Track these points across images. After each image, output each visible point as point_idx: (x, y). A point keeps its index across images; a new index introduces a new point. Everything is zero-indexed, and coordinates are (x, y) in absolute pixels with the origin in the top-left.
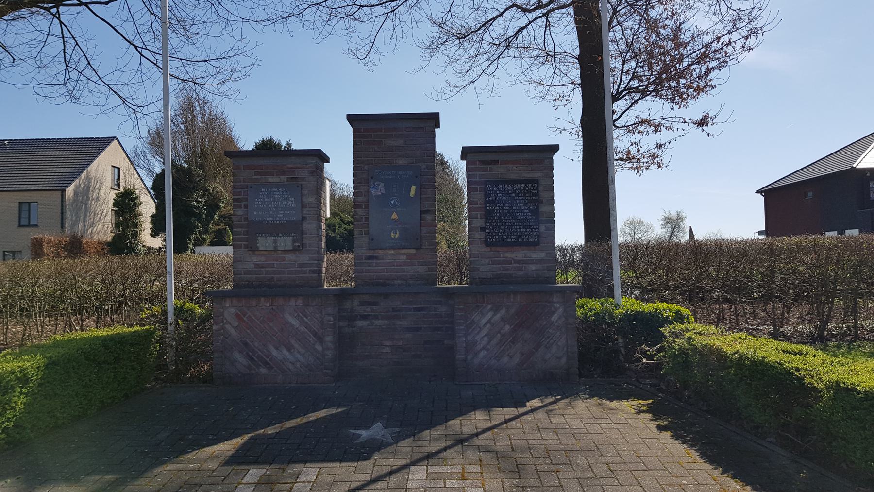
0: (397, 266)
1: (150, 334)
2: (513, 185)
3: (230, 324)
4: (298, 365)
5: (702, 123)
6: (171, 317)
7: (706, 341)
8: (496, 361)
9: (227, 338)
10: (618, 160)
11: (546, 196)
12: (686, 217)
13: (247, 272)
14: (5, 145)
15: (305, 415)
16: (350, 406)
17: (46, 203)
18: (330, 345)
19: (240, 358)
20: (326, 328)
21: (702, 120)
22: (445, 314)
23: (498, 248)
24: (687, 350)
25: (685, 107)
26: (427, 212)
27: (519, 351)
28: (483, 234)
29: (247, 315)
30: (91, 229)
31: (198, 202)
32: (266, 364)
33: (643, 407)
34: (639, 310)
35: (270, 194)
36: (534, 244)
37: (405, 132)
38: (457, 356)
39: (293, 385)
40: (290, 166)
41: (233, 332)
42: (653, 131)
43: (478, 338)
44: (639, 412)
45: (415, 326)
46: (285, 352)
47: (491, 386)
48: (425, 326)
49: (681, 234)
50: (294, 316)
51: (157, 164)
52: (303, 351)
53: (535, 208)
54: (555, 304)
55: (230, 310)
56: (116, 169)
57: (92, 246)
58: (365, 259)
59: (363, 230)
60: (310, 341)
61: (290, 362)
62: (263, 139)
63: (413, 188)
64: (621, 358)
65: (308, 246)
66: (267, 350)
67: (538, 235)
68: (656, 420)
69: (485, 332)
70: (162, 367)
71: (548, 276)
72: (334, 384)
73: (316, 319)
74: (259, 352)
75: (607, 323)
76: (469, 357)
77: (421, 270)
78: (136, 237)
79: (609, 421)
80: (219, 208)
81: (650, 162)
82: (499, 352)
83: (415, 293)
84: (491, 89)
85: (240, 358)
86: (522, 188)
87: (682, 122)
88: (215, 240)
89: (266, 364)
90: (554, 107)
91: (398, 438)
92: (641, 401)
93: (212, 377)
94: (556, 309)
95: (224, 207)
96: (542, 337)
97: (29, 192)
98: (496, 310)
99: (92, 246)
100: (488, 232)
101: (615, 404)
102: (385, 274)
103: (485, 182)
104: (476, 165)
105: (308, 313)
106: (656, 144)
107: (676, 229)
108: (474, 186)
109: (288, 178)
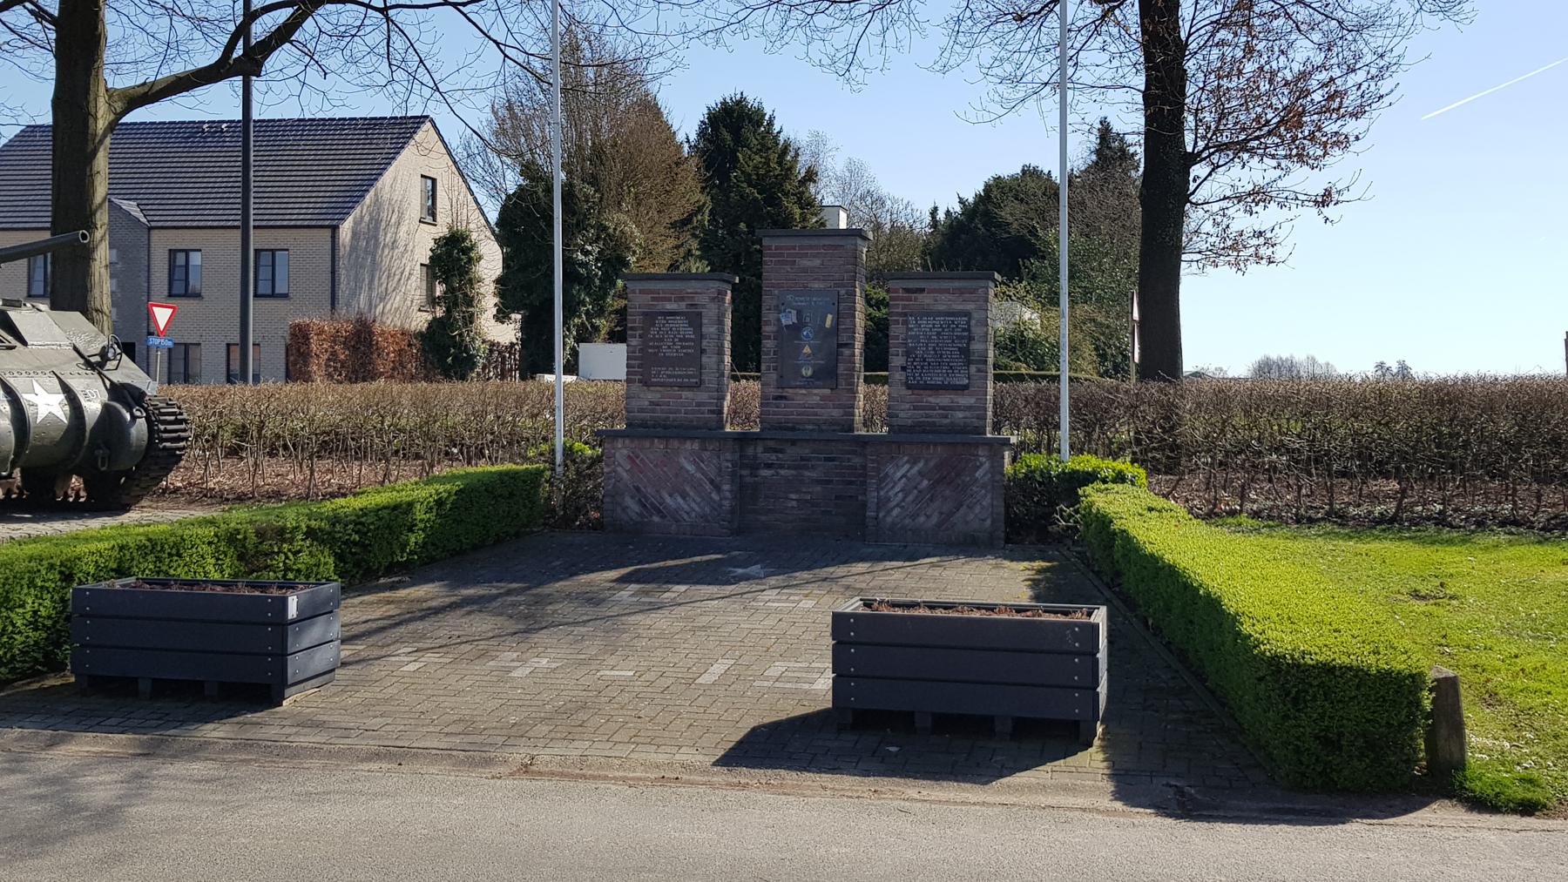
1: (540, 473)
4: (693, 515)
6: (559, 458)
13: (641, 410)
14: (222, 131)
18: (728, 494)
19: (633, 506)
23: (922, 392)
26: (846, 345)
31: (586, 253)
32: (659, 512)
43: (891, 493)
46: (680, 500)
51: (510, 175)
52: (699, 500)
55: (622, 450)
56: (429, 182)
62: (725, 99)
63: (830, 317)
76: (881, 515)
77: (836, 413)
78: (471, 323)
80: (626, 264)
85: (633, 506)
88: (618, 328)
89: (659, 512)
91: (767, 576)
94: (982, 464)
97: (286, 231)
98: (914, 462)
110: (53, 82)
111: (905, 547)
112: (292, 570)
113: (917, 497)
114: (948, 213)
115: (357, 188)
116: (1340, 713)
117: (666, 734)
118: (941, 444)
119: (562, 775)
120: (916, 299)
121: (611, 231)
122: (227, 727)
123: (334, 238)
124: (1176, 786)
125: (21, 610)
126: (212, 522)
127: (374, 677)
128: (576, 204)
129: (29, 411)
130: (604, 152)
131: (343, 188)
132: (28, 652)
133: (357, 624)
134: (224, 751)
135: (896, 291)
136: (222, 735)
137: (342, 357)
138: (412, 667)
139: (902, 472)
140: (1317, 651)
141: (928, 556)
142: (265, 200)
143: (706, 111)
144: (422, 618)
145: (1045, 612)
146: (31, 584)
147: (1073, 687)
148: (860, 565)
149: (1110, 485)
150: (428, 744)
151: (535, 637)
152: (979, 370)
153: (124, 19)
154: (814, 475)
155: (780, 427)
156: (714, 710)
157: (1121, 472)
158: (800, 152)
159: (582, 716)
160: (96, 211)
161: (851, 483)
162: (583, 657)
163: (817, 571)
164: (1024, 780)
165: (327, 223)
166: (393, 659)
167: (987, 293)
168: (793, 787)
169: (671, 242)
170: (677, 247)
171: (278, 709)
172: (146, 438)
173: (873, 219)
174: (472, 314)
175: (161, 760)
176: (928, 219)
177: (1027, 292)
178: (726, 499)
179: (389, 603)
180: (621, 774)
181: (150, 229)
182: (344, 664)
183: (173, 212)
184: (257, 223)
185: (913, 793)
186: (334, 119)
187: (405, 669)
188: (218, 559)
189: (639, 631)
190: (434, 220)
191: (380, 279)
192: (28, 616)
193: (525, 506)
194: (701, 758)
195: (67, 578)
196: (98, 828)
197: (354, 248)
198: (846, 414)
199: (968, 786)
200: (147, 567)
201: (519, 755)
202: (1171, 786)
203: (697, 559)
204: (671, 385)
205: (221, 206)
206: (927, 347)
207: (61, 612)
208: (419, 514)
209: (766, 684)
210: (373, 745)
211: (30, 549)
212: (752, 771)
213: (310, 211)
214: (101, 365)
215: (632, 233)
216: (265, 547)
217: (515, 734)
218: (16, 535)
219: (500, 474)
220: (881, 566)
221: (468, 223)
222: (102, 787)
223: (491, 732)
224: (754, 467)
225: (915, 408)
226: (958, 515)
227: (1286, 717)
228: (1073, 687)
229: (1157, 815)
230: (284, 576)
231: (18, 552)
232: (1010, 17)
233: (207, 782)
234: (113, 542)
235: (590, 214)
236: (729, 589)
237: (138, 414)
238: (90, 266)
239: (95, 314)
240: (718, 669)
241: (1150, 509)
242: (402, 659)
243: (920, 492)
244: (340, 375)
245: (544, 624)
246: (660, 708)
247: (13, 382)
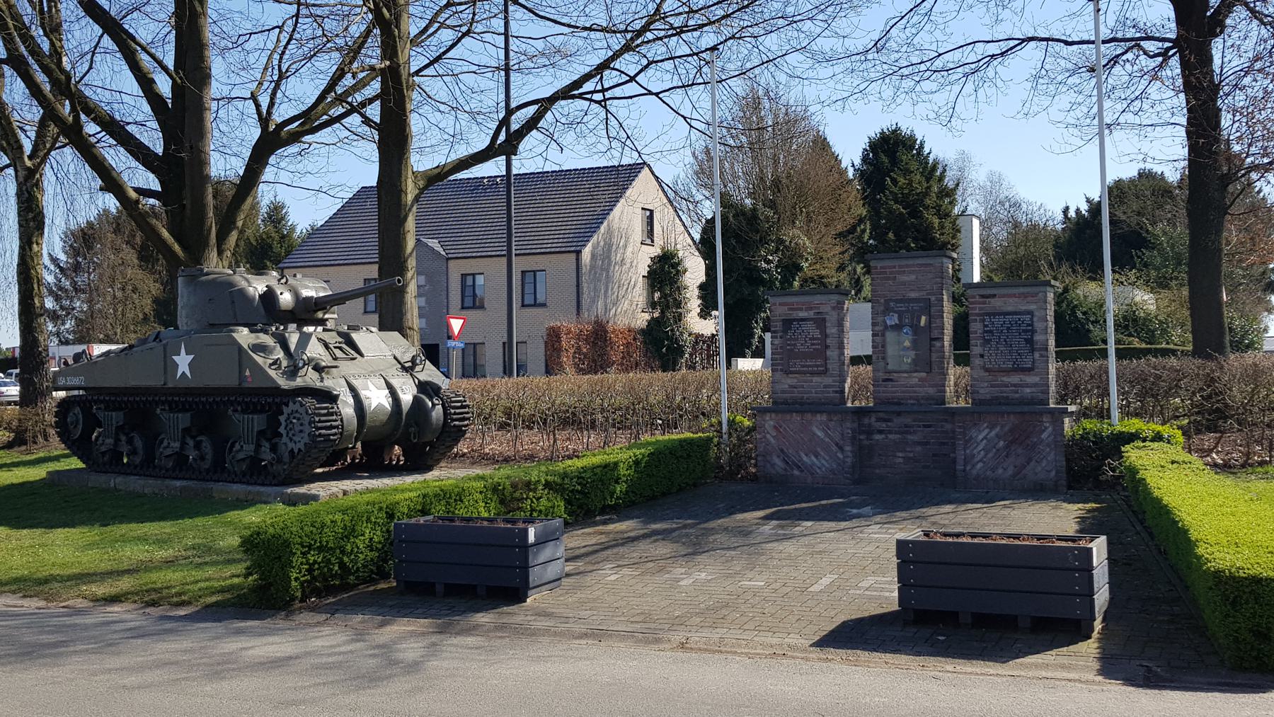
1: (710, 439)
4: (824, 469)
6: (725, 428)
13: (783, 392)
14: (497, 184)
17: (556, 269)
18: (849, 454)
19: (777, 461)
30: (614, 309)
31: (769, 262)
41: (772, 440)
43: (975, 451)
46: (813, 458)
52: (827, 458)
55: (769, 422)
57: (620, 336)
62: (882, 130)
77: (931, 391)
78: (680, 320)
80: (800, 269)
85: (777, 461)
91: (874, 514)
94: (1046, 428)
97: (544, 256)
98: (992, 428)
99: (620, 336)
110: (378, 163)
111: (987, 492)
112: (535, 511)
114: (1078, 211)
115: (595, 221)
116: (1268, 613)
117: (781, 625)
118: (1014, 413)
119: (706, 650)
120: (989, 303)
121: (787, 243)
122: (491, 615)
123: (578, 260)
124: (1147, 666)
125: (362, 538)
126: (482, 478)
127: (588, 584)
128: (759, 224)
129: (366, 403)
130: (780, 182)
131: (584, 222)
132: (367, 566)
133: (579, 548)
134: (489, 631)
135: (974, 297)
136: (487, 620)
137: (585, 350)
138: (613, 578)
139: (983, 435)
140: (1250, 567)
141: (1003, 499)
142: (528, 234)
143: (868, 140)
144: (622, 544)
145: (1057, 540)
146: (368, 520)
147: (1075, 595)
148: (948, 506)
149: (1148, 444)
150: (620, 629)
151: (699, 558)
152: (1041, 356)
153: (424, 119)
155: (889, 402)
156: (817, 609)
157: (1158, 432)
158: (947, 169)
159: (724, 612)
160: (408, 258)
161: (944, 444)
162: (730, 572)
163: (912, 511)
164: (1033, 660)
165: (572, 249)
166: (601, 572)
167: (1046, 296)
168: (865, 661)
169: (838, 249)
170: (842, 253)
171: (524, 604)
172: (442, 419)
173: (1011, 220)
174: (681, 314)
175: (449, 635)
176: (1060, 217)
177: (1137, 278)
178: (848, 457)
179: (602, 533)
180: (746, 651)
181: (448, 259)
182: (568, 575)
183: (463, 246)
184: (518, 252)
185: (950, 668)
186: (577, 170)
187: (609, 578)
188: (486, 503)
189: (773, 554)
190: (653, 241)
191: (612, 289)
192: (367, 542)
193: (699, 464)
194: (803, 641)
195: (391, 516)
196: (409, 673)
197: (593, 267)
199: (991, 664)
200: (439, 509)
201: (678, 637)
202: (1143, 666)
203: (824, 502)
204: (805, 373)
205: (497, 240)
206: (1000, 338)
207: (387, 539)
208: (623, 471)
209: (858, 592)
210: (578, 628)
211: (367, 497)
212: (837, 650)
213: (561, 240)
214: (412, 368)
216: (517, 495)
217: (678, 623)
218: (359, 487)
219: (680, 441)
220: (964, 507)
221: (676, 244)
222: (411, 650)
223: (661, 621)
224: (869, 432)
225: (992, 386)
226: (1028, 468)
227: (1227, 616)
228: (1075, 595)
229: (1124, 684)
230: (531, 515)
231: (361, 500)
232: (1084, 69)
233: (476, 648)
234: (419, 492)
235: (771, 231)
236: (843, 524)
237: (437, 402)
238: (404, 297)
239: (408, 331)
240: (825, 581)
241: (1173, 462)
242: (607, 572)
244: (584, 364)
245: (706, 549)
246: (779, 607)
247: (355, 383)
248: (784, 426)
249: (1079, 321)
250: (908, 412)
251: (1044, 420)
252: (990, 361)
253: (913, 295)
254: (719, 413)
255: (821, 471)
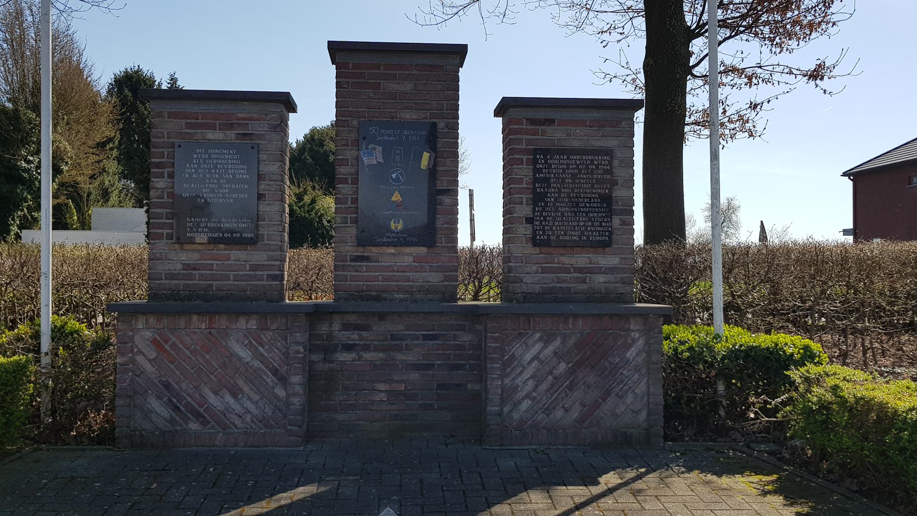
0: (398, 272)
1: (20, 369)
2: (575, 157)
3: (144, 355)
4: (248, 418)
5: (816, 75)
6: (46, 344)
7: (861, 392)
8: (545, 416)
9: (138, 376)
10: (693, 124)
11: (622, 174)
12: (739, 207)
13: (171, 276)
15: (272, 495)
16: (336, 482)
18: (298, 389)
19: (157, 406)
20: (293, 364)
21: (815, 70)
22: (469, 344)
24: (830, 403)
25: (788, 51)
27: (579, 401)
28: (529, 226)
29: (170, 343)
31: (29, 162)
32: (198, 415)
33: (768, 485)
34: (751, 344)
35: (210, 158)
36: (605, 245)
37: (416, 72)
38: (489, 408)
39: (239, 449)
40: (240, 115)
41: (148, 367)
42: (746, 84)
43: (519, 381)
44: (765, 493)
45: (424, 362)
46: (229, 398)
47: (538, 453)
48: (439, 362)
49: (733, 231)
50: (243, 344)
52: (256, 397)
53: (607, 191)
54: (633, 334)
58: (351, 261)
59: (349, 216)
60: (267, 383)
61: (236, 414)
62: (126, 69)
64: (722, 413)
65: (266, 237)
66: (201, 395)
67: (609, 232)
68: (791, 505)
69: (531, 373)
70: (34, 417)
71: (623, 292)
72: (302, 448)
73: (277, 349)
74: (188, 398)
75: (706, 362)
77: (435, 278)
79: (724, 506)
81: (738, 129)
82: (549, 403)
83: (425, 313)
84: (502, 12)
85: (157, 406)
86: (589, 162)
87: (787, 73)
89: (198, 415)
90: (602, 42)
92: (761, 477)
93: (114, 435)
94: (634, 341)
95: (68, 171)
96: (612, 382)
98: (547, 340)
100: (537, 225)
101: (725, 481)
102: (381, 283)
103: (535, 152)
104: (523, 125)
105: (266, 340)
106: (749, 103)
107: (725, 224)
108: (518, 157)
109: (238, 134)
113: (552, 385)
143: (113, 77)
154: (410, 357)
155: (361, 296)
161: (457, 367)
178: (295, 394)
198: (447, 279)
206: (560, 191)
215: (65, 148)
224: (328, 348)
235: (33, 132)
243: (555, 378)
248: (174, 339)
249: (325, 228)
250: (400, 314)
251: (632, 327)
252: (544, 230)
253: (407, 116)
254: (34, 317)
255: (243, 422)
